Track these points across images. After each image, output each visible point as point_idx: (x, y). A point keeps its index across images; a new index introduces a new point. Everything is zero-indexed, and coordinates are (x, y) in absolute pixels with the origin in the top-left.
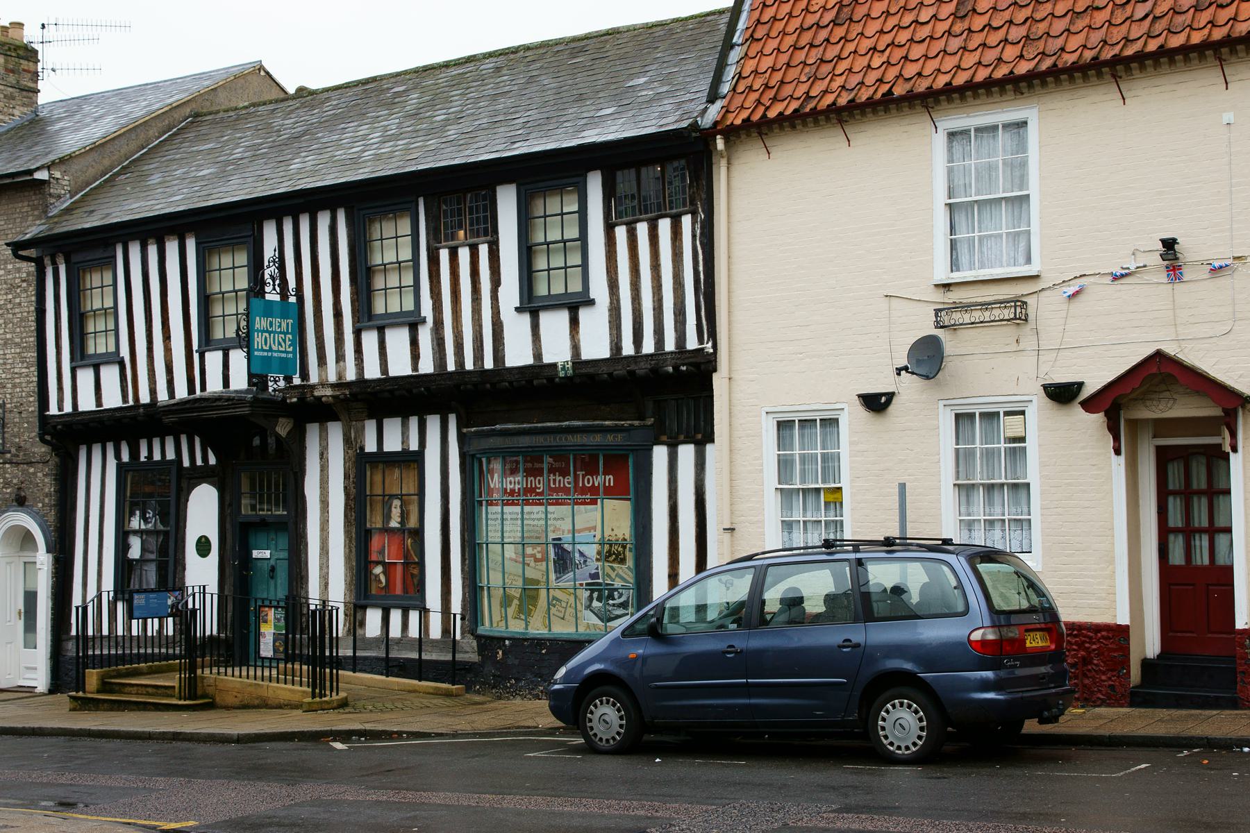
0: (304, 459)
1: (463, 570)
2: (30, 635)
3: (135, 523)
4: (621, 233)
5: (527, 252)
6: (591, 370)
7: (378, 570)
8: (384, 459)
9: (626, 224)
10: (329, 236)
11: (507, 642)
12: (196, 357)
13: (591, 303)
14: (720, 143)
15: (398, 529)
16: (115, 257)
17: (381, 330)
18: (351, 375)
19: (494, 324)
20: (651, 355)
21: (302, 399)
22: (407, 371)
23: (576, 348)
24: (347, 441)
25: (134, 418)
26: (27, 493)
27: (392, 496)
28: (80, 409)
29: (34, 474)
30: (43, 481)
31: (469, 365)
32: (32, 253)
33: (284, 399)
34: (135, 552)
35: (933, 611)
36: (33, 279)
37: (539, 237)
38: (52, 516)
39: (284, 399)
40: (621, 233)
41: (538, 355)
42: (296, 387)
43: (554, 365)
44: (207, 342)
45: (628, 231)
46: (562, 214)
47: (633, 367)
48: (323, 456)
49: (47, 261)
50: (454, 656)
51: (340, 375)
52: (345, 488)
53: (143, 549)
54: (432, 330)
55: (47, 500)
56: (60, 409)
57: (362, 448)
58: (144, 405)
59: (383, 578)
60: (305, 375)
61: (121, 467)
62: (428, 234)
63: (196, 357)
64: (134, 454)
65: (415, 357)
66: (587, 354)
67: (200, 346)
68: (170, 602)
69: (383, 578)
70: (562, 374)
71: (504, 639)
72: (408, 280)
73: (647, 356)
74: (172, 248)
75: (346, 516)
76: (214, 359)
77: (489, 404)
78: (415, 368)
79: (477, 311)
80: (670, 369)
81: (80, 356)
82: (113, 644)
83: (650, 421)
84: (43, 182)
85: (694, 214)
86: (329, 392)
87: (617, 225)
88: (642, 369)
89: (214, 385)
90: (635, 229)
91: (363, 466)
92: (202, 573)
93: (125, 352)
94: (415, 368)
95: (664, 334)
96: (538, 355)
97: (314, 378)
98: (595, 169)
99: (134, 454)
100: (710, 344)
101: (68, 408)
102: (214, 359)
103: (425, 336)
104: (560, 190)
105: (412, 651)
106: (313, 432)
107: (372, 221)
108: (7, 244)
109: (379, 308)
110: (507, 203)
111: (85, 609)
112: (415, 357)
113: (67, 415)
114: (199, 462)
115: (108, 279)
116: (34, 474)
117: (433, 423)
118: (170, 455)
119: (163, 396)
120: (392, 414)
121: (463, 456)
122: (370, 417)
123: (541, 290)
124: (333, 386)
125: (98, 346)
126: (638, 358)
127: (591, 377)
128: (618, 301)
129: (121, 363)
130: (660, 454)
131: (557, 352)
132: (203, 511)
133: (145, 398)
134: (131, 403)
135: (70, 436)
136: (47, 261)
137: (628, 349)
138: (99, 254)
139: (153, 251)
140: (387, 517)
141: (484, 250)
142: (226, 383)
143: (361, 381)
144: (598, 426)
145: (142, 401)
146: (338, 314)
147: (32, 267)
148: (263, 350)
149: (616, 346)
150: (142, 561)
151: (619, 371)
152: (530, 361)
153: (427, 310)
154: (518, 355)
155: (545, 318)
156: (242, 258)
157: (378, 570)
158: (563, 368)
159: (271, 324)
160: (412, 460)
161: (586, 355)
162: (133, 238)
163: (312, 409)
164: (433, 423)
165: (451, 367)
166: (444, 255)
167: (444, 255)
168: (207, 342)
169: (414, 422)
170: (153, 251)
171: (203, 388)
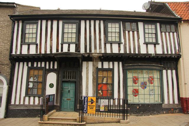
1: (123, 92)
3: (31, 80)
7: (100, 91)
8: (103, 70)
13: (122, 43)
16: (38, 23)
18: (103, 52)
19: (138, 46)
21: (89, 56)
22: (145, 52)
24: (93, 65)
25: (39, 57)
30: (8, 69)
34: (31, 85)
36: (136, 25)
37: (27, 31)
38: (9, 77)
40: (163, 34)
42: (88, 53)
43: (151, 54)
47: (166, 56)
55: (7, 73)
57: (97, 67)
58: (43, 54)
61: (28, 67)
62: (123, 28)
64: (33, 65)
65: (120, 50)
70: (153, 56)
71: (139, 104)
72: (34, 36)
74: (92, 22)
75: (93, 81)
76: (108, 46)
79: (171, 43)
85: (176, 32)
86: (97, 55)
88: (168, 56)
91: (97, 70)
93: (38, 42)
95: (171, 51)
98: (158, 23)
99: (33, 65)
101: (18, 53)
103: (122, 46)
104: (33, 23)
108: (9, 16)
110: (141, 25)
112: (120, 50)
114: (51, 67)
120: (106, 61)
121: (123, 70)
122: (101, 61)
127: (158, 57)
129: (37, 45)
132: (52, 78)
133: (43, 52)
135: (16, 60)
137: (166, 53)
138: (34, 21)
140: (103, 81)
141: (136, 33)
142: (69, 50)
143: (106, 53)
146: (100, 40)
149: (163, 52)
151: (164, 56)
152: (146, 53)
153: (123, 41)
154: (143, 51)
155: (149, 46)
160: (112, 70)
161: (157, 53)
162: (44, 19)
163: (88, 58)
166: (127, 32)
171: (62, 50)
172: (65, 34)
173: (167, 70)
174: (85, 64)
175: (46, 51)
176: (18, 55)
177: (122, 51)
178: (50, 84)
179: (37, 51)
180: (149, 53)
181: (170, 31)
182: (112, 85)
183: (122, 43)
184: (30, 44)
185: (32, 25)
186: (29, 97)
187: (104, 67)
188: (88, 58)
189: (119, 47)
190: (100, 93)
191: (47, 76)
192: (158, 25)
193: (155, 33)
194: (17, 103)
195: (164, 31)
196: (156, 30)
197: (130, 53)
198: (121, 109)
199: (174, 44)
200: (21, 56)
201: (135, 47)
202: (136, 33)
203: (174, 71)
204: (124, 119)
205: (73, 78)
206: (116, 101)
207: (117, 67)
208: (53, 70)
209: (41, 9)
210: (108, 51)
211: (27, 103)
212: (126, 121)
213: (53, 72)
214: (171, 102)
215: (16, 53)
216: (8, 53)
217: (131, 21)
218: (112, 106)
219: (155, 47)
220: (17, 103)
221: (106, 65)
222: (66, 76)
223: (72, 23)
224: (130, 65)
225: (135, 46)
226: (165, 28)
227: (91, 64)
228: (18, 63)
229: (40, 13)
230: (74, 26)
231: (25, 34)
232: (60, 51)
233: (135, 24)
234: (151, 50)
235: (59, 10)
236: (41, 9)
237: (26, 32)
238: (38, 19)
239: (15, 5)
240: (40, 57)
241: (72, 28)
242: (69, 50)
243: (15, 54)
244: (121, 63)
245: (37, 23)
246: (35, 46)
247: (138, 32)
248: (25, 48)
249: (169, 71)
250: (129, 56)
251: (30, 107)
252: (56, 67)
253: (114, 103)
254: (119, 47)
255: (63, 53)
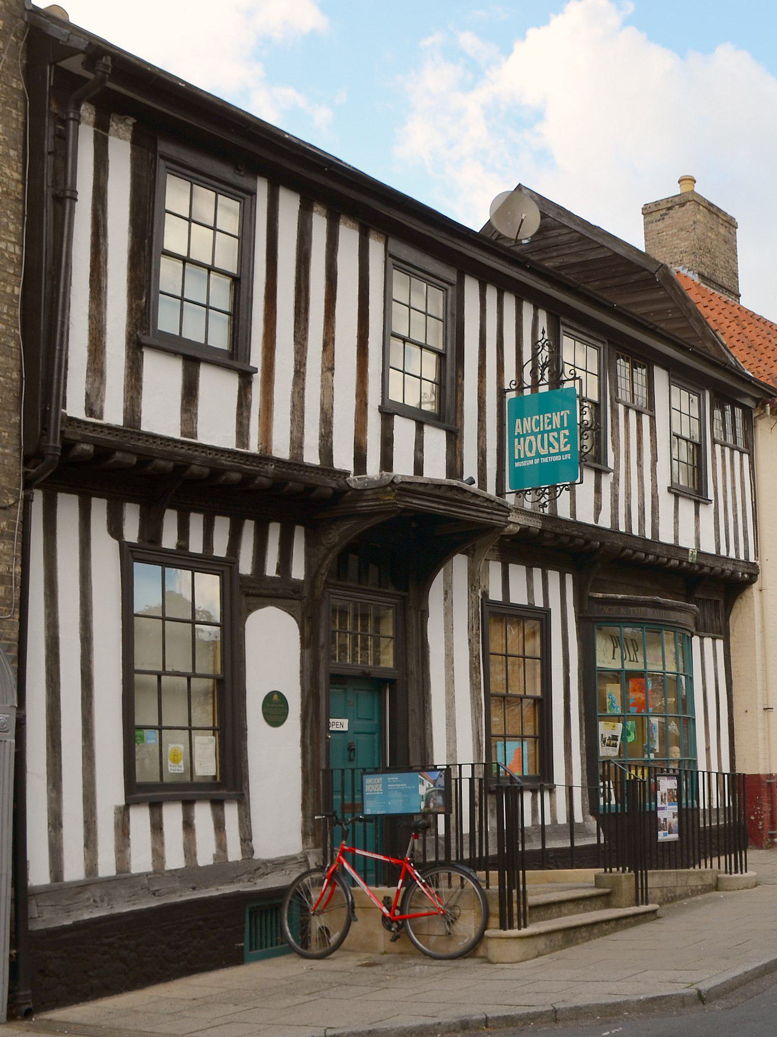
13: (607, 472)
25: (248, 477)
35: (189, 765)
50: (572, 843)
57: (485, 594)
58: (279, 461)
65: (598, 508)
88: (266, 475)
91: (492, 615)
112: (598, 508)
114: (271, 570)
121: (579, 620)
124: (544, 517)
130: (696, 640)
131: (161, 417)
141: (646, 419)
144: (612, 598)
148: (526, 458)
159: (538, 423)
171: (387, 462)
173: (702, 638)
176: (109, 428)
183: (255, 370)
186: (156, 807)
193: (233, 268)
194: (74, 871)
197: (296, 464)
202: (646, 419)
203: (720, 643)
208: (279, 593)
209: (74, 19)
211: (141, 861)
215: (90, 411)
220: (74, 871)
224: (620, 596)
233: (644, 371)
244: (569, 578)
247: (653, 418)
251: (174, 891)
252: (298, 572)
255: (102, 426)
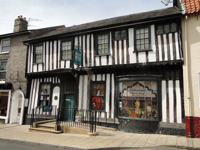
0: (79, 82)
1: (114, 104)
2: (19, 113)
3: (42, 93)
4: (159, 37)
5: (135, 40)
6: (151, 64)
7: (94, 104)
8: (96, 82)
9: (160, 35)
10: (90, 39)
11: (128, 120)
12: (59, 62)
14: (186, 17)
15: (99, 96)
16: (43, 44)
17: (100, 57)
19: (127, 55)
20: (167, 61)
21: (81, 70)
23: (147, 60)
24: (88, 78)
26: (22, 87)
27: (98, 90)
28: (34, 72)
29: (23, 84)
30: (24, 85)
31: (121, 63)
32: (26, 44)
33: (77, 70)
34: (42, 99)
38: (25, 92)
39: (77, 70)
40: (159, 37)
41: (137, 61)
43: (142, 63)
44: (61, 59)
45: (161, 36)
46: (140, 34)
48: (83, 81)
49: (29, 46)
51: (90, 65)
52: (88, 88)
53: (43, 98)
54: (112, 57)
56: (30, 72)
57: (92, 80)
59: (95, 105)
60: (82, 65)
63: (59, 62)
64: (43, 80)
65: (108, 62)
66: (103, 64)
67: (60, 60)
68: (50, 108)
69: (95, 105)
70: (144, 65)
73: (166, 61)
74: (47, 43)
76: (63, 63)
77: (121, 71)
78: (108, 64)
80: (172, 64)
81: (34, 62)
82: (36, 116)
83: (162, 76)
84: (30, 33)
85: (178, 32)
86: (87, 69)
87: (158, 35)
89: (62, 67)
90: (163, 36)
91: (92, 84)
92: (56, 103)
94: (108, 64)
96: (137, 61)
97: (84, 66)
99: (43, 80)
100: (183, 59)
102: (63, 63)
105: (104, 120)
106: (81, 77)
107: (98, 36)
109: (99, 53)
110: (131, 32)
111: (34, 110)
112: (108, 62)
113: (31, 73)
114: (56, 82)
115: (42, 48)
116: (23, 84)
117: (108, 76)
118: (50, 81)
119: (161, 59)
122: (94, 74)
123: (138, 47)
124: (88, 67)
125: (39, 61)
126: (163, 61)
127: (151, 66)
128: (158, 50)
129: (43, 64)
132: (57, 92)
133: (47, 70)
134: (44, 71)
135: (31, 77)
136: (29, 46)
137: (161, 59)
138: (41, 44)
139: (51, 43)
141: (125, 41)
142: (65, 66)
145: (47, 70)
147: (27, 47)
150: (43, 101)
151: (158, 64)
152: (135, 62)
154: (133, 61)
156: (70, 43)
157: (94, 104)
158: (144, 64)
160: (104, 83)
161: (150, 61)
163: (83, 72)
164: (108, 76)
165: (116, 63)
166: (116, 42)
167: (116, 42)
168: (61, 59)
169: (104, 75)
170: (51, 43)
171: (60, 67)
172: (137, 41)
174: (81, 77)
175: (49, 69)
177: (110, 63)
178: (55, 97)
179: (43, 70)
180: (140, 62)
181: (162, 32)
182: (104, 98)
184: (148, 52)
185: (139, 30)
187: (97, 80)
188: (83, 72)
189: (108, 58)
190: (94, 105)
191: (54, 90)
192: (153, 28)
195: (161, 34)
196: (136, 38)
197: (119, 65)
198: (97, 122)
199: (173, 48)
200: (33, 74)
201: (124, 57)
202: (125, 41)
203: (178, 82)
204: (92, 132)
205: (72, 91)
206: (108, 114)
207: (109, 79)
210: (98, 64)
212: (94, 133)
213: (53, 88)
214: (172, 120)
216: (24, 72)
217: (120, 29)
218: (84, 118)
219: (147, 54)
221: (99, 78)
222: (70, 89)
223: (68, 41)
225: (124, 56)
226: (162, 30)
227: (86, 77)
228: (95, 75)
229: (65, 31)
230: (70, 43)
231: (98, 45)
232: (59, 68)
234: (142, 59)
235: (74, 26)
236: (66, 27)
237: (98, 44)
238: (43, 42)
239: (30, 32)
240: (152, 66)
241: (144, 33)
242: (65, 66)
243: (29, 73)
244: (113, 75)
245: (42, 45)
246: (42, 64)
248: (35, 67)
249: (171, 82)
250: (117, 68)
253: (106, 116)
254: (108, 58)
